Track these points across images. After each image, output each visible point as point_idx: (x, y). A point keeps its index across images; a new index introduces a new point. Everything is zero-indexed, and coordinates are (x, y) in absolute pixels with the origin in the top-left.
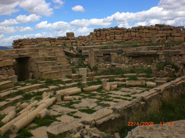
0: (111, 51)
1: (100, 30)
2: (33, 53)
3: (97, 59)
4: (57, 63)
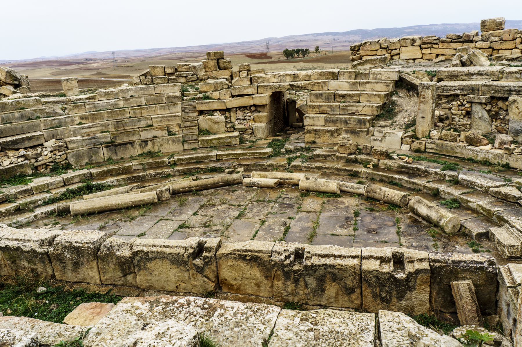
0: (516, 91)
2: (318, 83)
3: (469, 110)
4: (348, 110)
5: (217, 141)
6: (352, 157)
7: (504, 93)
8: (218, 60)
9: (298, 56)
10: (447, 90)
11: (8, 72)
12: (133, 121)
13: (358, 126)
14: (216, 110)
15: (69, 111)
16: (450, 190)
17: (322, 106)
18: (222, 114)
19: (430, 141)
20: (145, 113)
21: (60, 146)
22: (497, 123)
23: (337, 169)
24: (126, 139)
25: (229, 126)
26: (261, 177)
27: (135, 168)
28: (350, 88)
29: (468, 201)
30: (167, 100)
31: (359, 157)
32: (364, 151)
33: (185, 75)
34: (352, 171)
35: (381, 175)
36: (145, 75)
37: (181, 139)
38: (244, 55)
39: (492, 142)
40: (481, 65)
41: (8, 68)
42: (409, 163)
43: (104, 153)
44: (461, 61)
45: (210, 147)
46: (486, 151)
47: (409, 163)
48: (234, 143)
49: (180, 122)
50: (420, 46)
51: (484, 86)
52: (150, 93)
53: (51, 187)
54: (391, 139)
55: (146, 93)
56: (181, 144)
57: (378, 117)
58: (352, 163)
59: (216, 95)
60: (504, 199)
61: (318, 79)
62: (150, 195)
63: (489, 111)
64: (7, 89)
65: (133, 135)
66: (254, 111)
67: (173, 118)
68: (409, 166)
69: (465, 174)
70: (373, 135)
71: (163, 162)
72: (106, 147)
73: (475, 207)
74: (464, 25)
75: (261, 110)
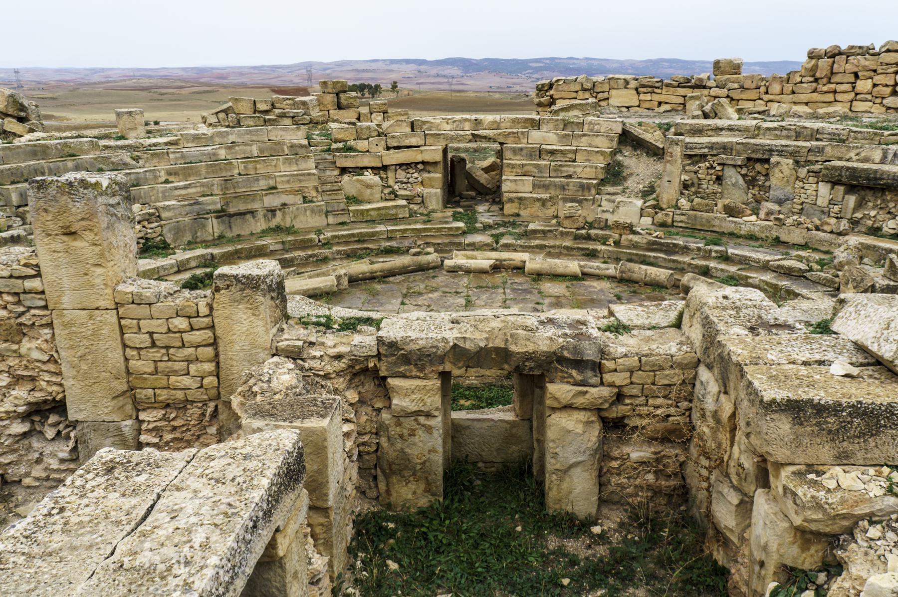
0: (779, 151)
1: (834, 54)
2: (514, 133)
3: (720, 174)
4: (562, 172)
5: (376, 213)
6: (583, 232)
7: (764, 154)
8: (337, 94)
9: (363, 95)
10: (691, 148)
11: (12, 96)
12: (248, 180)
13: (580, 193)
14: (366, 168)
15: (146, 162)
16: (723, 266)
17: (526, 165)
18: (375, 174)
19: (678, 212)
20: (262, 169)
21: (151, 215)
22: (755, 191)
23: (567, 248)
24: (242, 207)
25: (387, 191)
26: (468, 258)
27: (272, 248)
28: (559, 142)
29: (747, 277)
30: (291, 151)
31: (593, 232)
32: (596, 225)
33: (292, 115)
34: (588, 249)
35: (630, 254)
36: (226, 111)
37: (324, 208)
38: (267, 90)
39: (756, 212)
40: (729, 118)
41: (8, 92)
42: (660, 238)
43: (214, 227)
44: (703, 111)
45: (366, 221)
46: (750, 222)
47: (660, 238)
48: (401, 216)
49: (316, 184)
50: (636, 89)
51: (739, 144)
52: (260, 138)
53: (162, 273)
54: (627, 208)
55: (254, 138)
56: (324, 216)
57: (603, 182)
58: (585, 239)
59: (362, 145)
60: (788, 273)
61: (510, 128)
62: (326, 281)
63: (744, 176)
64: (11, 125)
65: (253, 200)
66: (422, 170)
67: (307, 177)
68: (663, 241)
69: (733, 248)
70: (600, 206)
71: (311, 240)
72: (217, 217)
73: (757, 283)
74: (617, 61)
75: (431, 169)
